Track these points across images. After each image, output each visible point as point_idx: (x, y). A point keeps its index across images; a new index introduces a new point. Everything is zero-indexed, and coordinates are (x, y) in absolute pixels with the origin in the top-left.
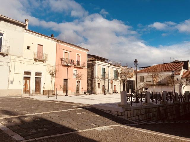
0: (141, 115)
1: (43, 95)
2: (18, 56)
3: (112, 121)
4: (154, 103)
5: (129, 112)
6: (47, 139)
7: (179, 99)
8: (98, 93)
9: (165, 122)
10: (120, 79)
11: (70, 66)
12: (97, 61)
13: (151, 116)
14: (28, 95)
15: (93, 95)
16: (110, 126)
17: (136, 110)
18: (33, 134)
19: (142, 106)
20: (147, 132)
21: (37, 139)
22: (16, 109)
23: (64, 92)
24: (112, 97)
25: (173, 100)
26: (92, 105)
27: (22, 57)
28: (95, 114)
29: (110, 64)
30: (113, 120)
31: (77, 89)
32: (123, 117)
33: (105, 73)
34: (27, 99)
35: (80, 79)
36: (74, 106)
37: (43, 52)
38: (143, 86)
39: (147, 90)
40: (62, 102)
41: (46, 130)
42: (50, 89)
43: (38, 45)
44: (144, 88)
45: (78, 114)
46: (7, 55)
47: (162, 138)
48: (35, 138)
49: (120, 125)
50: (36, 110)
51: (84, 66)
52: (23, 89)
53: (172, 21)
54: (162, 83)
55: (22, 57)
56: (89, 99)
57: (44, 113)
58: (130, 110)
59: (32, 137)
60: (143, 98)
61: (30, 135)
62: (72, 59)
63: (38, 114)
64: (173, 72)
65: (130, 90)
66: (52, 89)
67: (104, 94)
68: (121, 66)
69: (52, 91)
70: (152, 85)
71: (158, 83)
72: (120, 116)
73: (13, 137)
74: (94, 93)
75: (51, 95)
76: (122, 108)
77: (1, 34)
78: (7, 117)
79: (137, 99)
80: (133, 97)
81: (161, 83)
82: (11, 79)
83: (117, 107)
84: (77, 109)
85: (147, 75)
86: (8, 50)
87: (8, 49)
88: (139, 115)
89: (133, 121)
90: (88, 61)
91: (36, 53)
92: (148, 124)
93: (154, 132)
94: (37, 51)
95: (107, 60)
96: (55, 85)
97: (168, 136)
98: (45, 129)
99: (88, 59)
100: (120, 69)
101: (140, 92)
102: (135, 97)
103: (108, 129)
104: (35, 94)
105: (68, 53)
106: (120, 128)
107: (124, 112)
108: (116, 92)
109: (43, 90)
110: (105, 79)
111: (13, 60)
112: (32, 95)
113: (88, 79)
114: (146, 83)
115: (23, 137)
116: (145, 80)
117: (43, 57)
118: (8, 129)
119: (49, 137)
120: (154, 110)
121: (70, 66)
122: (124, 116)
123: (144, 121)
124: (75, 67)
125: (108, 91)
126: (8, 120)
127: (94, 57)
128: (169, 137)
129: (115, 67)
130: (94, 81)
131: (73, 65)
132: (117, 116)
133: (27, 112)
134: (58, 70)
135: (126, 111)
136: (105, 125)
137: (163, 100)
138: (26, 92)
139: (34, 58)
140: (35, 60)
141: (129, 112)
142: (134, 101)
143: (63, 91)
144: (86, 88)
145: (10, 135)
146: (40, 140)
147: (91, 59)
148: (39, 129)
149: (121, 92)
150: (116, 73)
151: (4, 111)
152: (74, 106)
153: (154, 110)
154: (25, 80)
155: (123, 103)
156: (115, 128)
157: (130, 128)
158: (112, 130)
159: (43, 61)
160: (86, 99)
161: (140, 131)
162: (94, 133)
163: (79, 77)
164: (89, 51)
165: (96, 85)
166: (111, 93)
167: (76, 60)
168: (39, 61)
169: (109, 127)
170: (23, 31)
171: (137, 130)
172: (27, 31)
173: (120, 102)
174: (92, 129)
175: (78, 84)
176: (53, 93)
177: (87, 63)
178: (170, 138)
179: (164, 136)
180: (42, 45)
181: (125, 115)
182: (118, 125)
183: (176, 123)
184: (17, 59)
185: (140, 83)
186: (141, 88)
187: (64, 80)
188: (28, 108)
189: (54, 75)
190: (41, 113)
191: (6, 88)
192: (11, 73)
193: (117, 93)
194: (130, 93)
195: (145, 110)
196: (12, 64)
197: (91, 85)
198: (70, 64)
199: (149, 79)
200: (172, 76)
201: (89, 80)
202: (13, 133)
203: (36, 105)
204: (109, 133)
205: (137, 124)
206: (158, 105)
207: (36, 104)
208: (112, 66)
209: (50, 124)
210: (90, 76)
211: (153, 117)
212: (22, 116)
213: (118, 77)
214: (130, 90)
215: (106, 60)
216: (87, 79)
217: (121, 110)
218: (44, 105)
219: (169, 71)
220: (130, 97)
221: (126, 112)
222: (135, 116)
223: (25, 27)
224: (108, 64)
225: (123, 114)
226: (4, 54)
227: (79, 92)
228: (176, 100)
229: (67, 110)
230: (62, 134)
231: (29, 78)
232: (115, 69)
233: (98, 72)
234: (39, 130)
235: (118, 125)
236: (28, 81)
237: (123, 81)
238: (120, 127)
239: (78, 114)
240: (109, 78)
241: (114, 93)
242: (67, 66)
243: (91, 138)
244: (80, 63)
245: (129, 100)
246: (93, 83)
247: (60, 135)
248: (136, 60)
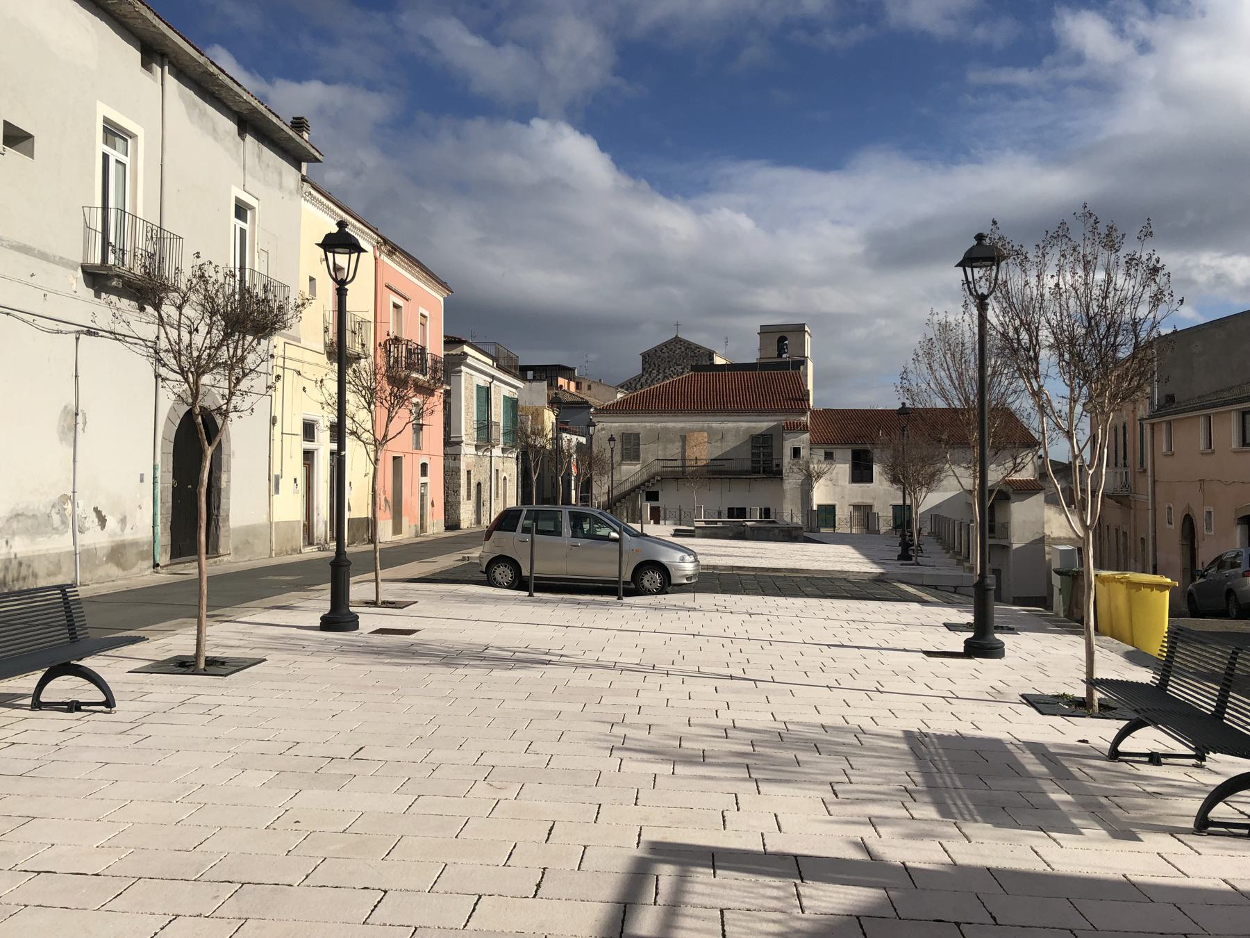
27: (300, 342)
38: (637, 480)
53: (603, 147)
54: (729, 466)
59: (819, 592)
71: (705, 468)
81: (723, 468)
185: (620, 465)
192: (78, 417)
199: (665, 449)
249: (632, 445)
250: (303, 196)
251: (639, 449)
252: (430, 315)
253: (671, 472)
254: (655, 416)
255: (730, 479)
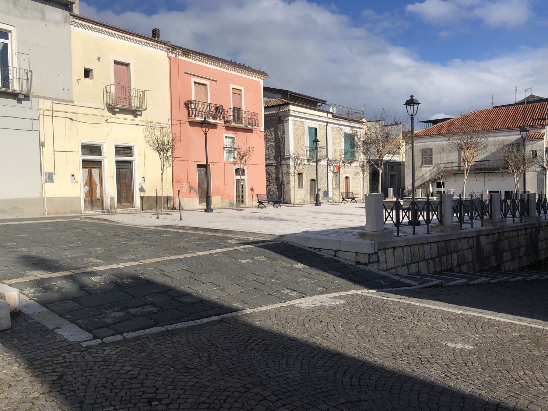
0: (425, 260)
1: (142, 210)
2: (60, 100)
3: (340, 281)
4: (463, 225)
5: (389, 252)
6: (156, 336)
7: (539, 213)
8: (297, 202)
9: (494, 278)
10: (361, 157)
11: (214, 126)
12: (291, 107)
13: (455, 263)
14: (99, 212)
15: (284, 207)
16: (337, 294)
17: (410, 246)
18: (115, 323)
19: (429, 235)
20: (445, 309)
21: (127, 337)
22: (66, 253)
23: (200, 202)
24: (340, 212)
25: (521, 214)
26: (281, 236)
27: (72, 102)
28: (292, 261)
29: (332, 113)
30: (343, 278)
31: (238, 191)
32: (373, 268)
33: (316, 141)
34: (98, 224)
35: (243, 162)
36: (230, 238)
37: (133, 86)
39: (442, 190)
40: (196, 229)
41: (152, 309)
42: (159, 194)
43: (116, 62)
44: (433, 183)
45: (243, 261)
46: (27, 97)
47: (492, 326)
48: (121, 333)
49: (364, 292)
50: (122, 253)
51: (253, 122)
52: (83, 197)
54: (487, 165)
55: (70, 102)
56: (271, 219)
57: (144, 261)
58: (394, 248)
59: (112, 332)
60: (433, 210)
61: (107, 326)
62: (219, 103)
63: (128, 264)
64: (523, 130)
65: (391, 191)
66: (165, 195)
67: (316, 205)
68: (364, 120)
69: (168, 199)
70: (457, 173)
71: (473, 168)
72: (366, 265)
73: (59, 332)
74: (287, 202)
75: (165, 211)
76: (368, 242)
77: (4, 34)
78: (40, 274)
79: (415, 216)
80: (403, 210)
82: (48, 168)
83: (356, 239)
84: (239, 248)
85: (444, 142)
86: (28, 83)
87: (28, 79)
88: (421, 261)
89: (402, 277)
90: (265, 108)
91: (112, 90)
92: (446, 285)
93: (466, 308)
94: (113, 82)
95: (323, 102)
96: (175, 181)
97: (506, 318)
98: (150, 309)
99: (265, 102)
100: (362, 128)
101: (419, 194)
102: (408, 209)
103: (332, 303)
104: (118, 208)
105: (205, 85)
106: (366, 299)
107: (375, 253)
108: (351, 196)
109: (142, 198)
110: (317, 161)
111: (46, 113)
112: (109, 212)
113: (269, 162)
114: (437, 167)
115: (89, 331)
116: (436, 159)
117: (132, 101)
118: (44, 309)
119: (162, 329)
120: (464, 244)
121: (214, 126)
122: (376, 265)
123: (432, 277)
124: (228, 128)
125: (326, 194)
126: (39, 283)
127: (284, 93)
128: (512, 324)
129: (346, 123)
130: (284, 169)
131: (222, 122)
132: (354, 264)
133: (96, 261)
134: (177, 136)
135: (383, 249)
136: (321, 293)
137: (491, 216)
138: (92, 204)
139: (107, 104)
140: (111, 109)
141: (389, 252)
142: (406, 220)
143: (197, 199)
144: (262, 188)
145: (51, 327)
146: (138, 338)
147: (275, 101)
148: (133, 308)
149: (366, 197)
150: (350, 139)
151: (32, 257)
152: (230, 238)
153: (464, 244)
154: (87, 171)
155: (372, 229)
156: (350, 301)
157: (395, 298)
158: (343, 305)
159: (135, 113)
160: (264, 218)
161: (425, 308)
162: (291, 316)
163: (242, 156)
164: (266, 75)
165: (292, 178)
166: (336, 199)
167: (229, 104)
168: (123, 111)
169: (334, 297)
170: (66, 21)
171: (417, 304)
172: (77, 21)
173: (364, 224)
174: (284, 305)
175: (238, 177)
176: (170, 205)
177: (262, 114)
178: (516, 325)
179: (498, 319)
180: (127, 65)
181: (378, 262)
182: (359, 292)
183: (529, 279)
184: (56, 107)
185: (421, 167)
186: (424, 184)
187: (199, 166)
188: (100, 249)
189: (169, 153)
190: (137, 263)
191: (37, 195)
193: (353, 199)
194: (391, 198)
195: (438, 247)
196: (45, 124)
197: (277, 179)
198: (214, 118)
200: (520, 144)
201: (271, 165)
202: (59, 320)
203: (121, 240)
204: (336, 316)
205: (416, 285)
206: (477, 231)
207: (123, 237)
208: (337, 122)
209: (164, 292)
210: (273, 153)
211: (459, 265)
212: (81, 271)
213: (356, 154)
214: (391, 191)
215: (319, 104)
216: (264, 162)
217: (367, 247)
218: (146, 240)
219: (509, 129)
220: (392, 210)
221: (381, 253)
222: (408, 264)
223: (72, 8)
224: (325, 115)
225: (374, 258)
226: (18, 94)
227: (243, 201)
228: (528, 214)
229: (211, 252)
230: (199, 322)
231: (98, 164)
232: (348, 130)
233: (297, 140)
234: (133, 311)
235: (359, 292)
236: (95, 172)
237: (371, 165)
238: (366, 296)
239: (243, 261)
240: (330, 157)
241: (344, 199)
242: (204, 124)
243: (283, 331)
244: (244, 116)
245: (389, 219)
246: (282, 174)
247: (192, 323)
248: (412, 96)
249: (428, 155)
250: (71, 25)
251: (432, 157)
252: (245, 89)
253: (452, 170)
254: (441, 137)
255: (484, 173)
